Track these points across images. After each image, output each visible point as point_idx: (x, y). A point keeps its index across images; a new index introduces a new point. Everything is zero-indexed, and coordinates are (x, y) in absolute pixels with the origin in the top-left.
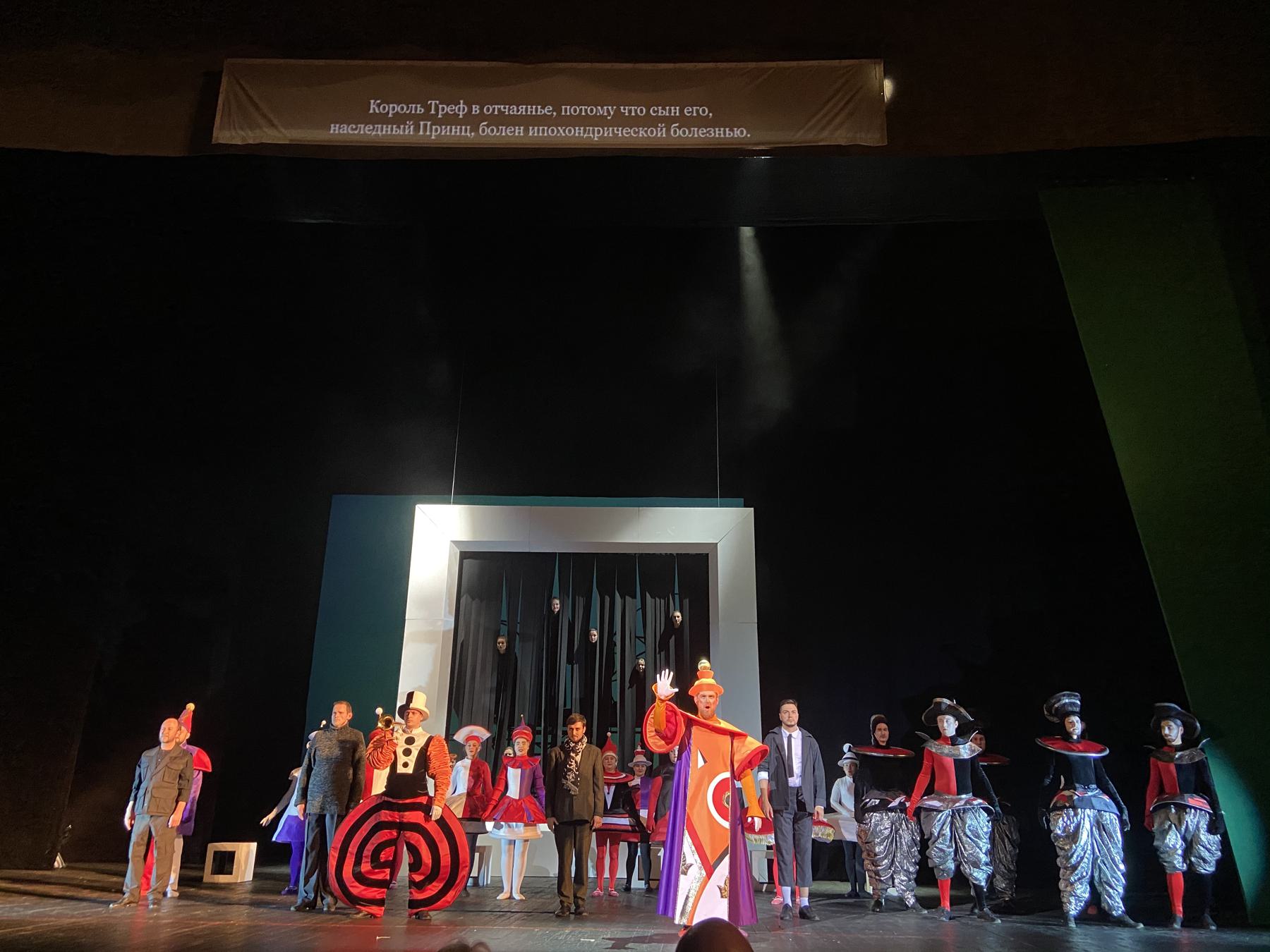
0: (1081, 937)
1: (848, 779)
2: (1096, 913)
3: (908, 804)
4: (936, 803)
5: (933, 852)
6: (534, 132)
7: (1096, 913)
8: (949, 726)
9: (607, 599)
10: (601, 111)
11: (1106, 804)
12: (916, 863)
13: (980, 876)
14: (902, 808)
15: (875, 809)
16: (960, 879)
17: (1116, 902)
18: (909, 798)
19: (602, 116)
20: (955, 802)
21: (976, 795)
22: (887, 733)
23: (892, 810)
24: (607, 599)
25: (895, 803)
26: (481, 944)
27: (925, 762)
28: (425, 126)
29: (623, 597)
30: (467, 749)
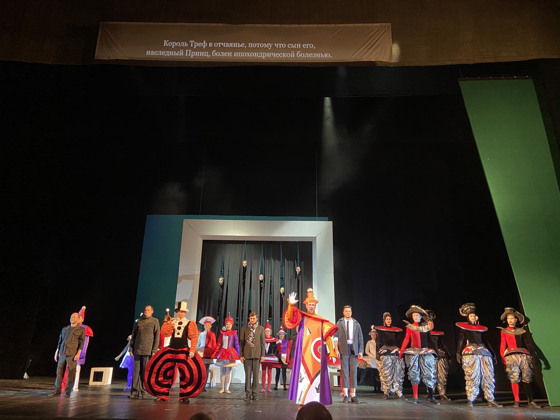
0: (475, 411)
3: (399, 352)
5: (410, 373)
7: (481, 399)
8: (417, 318)
12: (403, 378)
15: (385, 354)
16: (422, 385)
21: (430, 348)
23: (392, 355)
28: (188, 52)
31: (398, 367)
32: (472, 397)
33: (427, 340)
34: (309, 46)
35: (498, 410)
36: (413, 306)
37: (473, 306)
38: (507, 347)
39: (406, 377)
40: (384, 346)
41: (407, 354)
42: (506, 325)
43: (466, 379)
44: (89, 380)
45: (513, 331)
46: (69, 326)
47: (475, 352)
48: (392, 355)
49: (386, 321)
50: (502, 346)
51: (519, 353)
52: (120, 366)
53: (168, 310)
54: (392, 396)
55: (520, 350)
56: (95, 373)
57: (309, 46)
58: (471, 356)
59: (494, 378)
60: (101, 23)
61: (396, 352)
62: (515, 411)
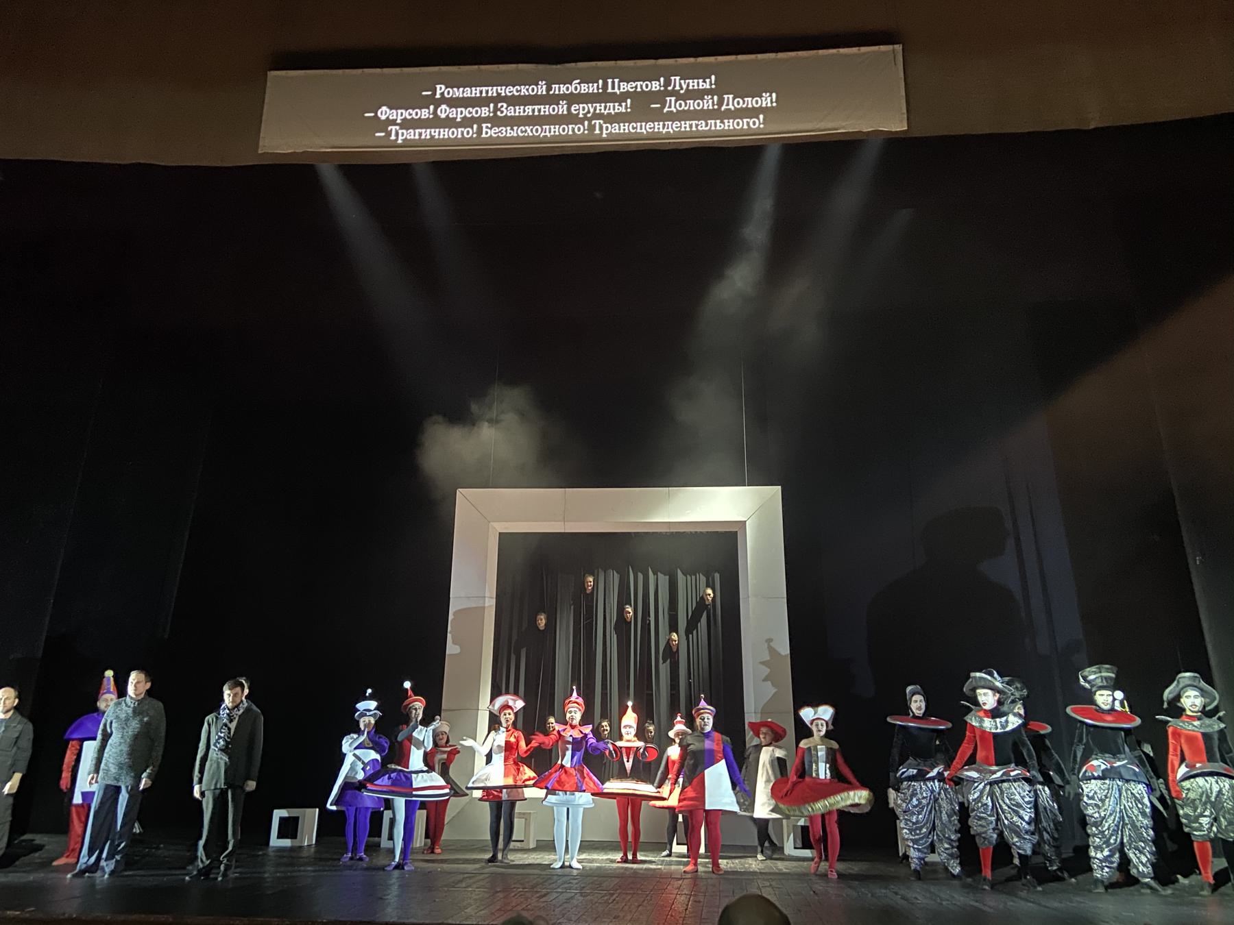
0: (1107, 906)
1: (721, 766)
2: (1125, 877)
3: (946, 774)
4: (974, 774)
5: (972, 822)
7: (1125, 877)
8: (988, 699)
9: (640, 576)
10: (412, 135)
11: (1135, 773)
12: (956, 831)
13: (1023, 846)
14: (940, 777)
15: (911, 778)
16: (1003, 849)
18: (948, 766)
22: (923, 705)
23: (932, 779)
24: (640, 576)
25: (933, 773)
26: (539, 917)
28: (613, 83)
29: (655, 573)
32: (1102, 872)
33: (1008, 750)
34: (748, 123)
37: (1107, 670)
38: (1183, 760)
39: (964, 828)
40: (911, 760)
42: (1176, 710)
45: (1196, 723)
47: (1107, 774)
48: (932, 779)
49: (914, 706)
50: (1173, 758)
51: (1211, 774)
52: (328, 806)
53: (407, 685)
54: (927, 873)
55: (1219, 766)
56: (282, 820)
57: (748, 123)
59: (91, 708)
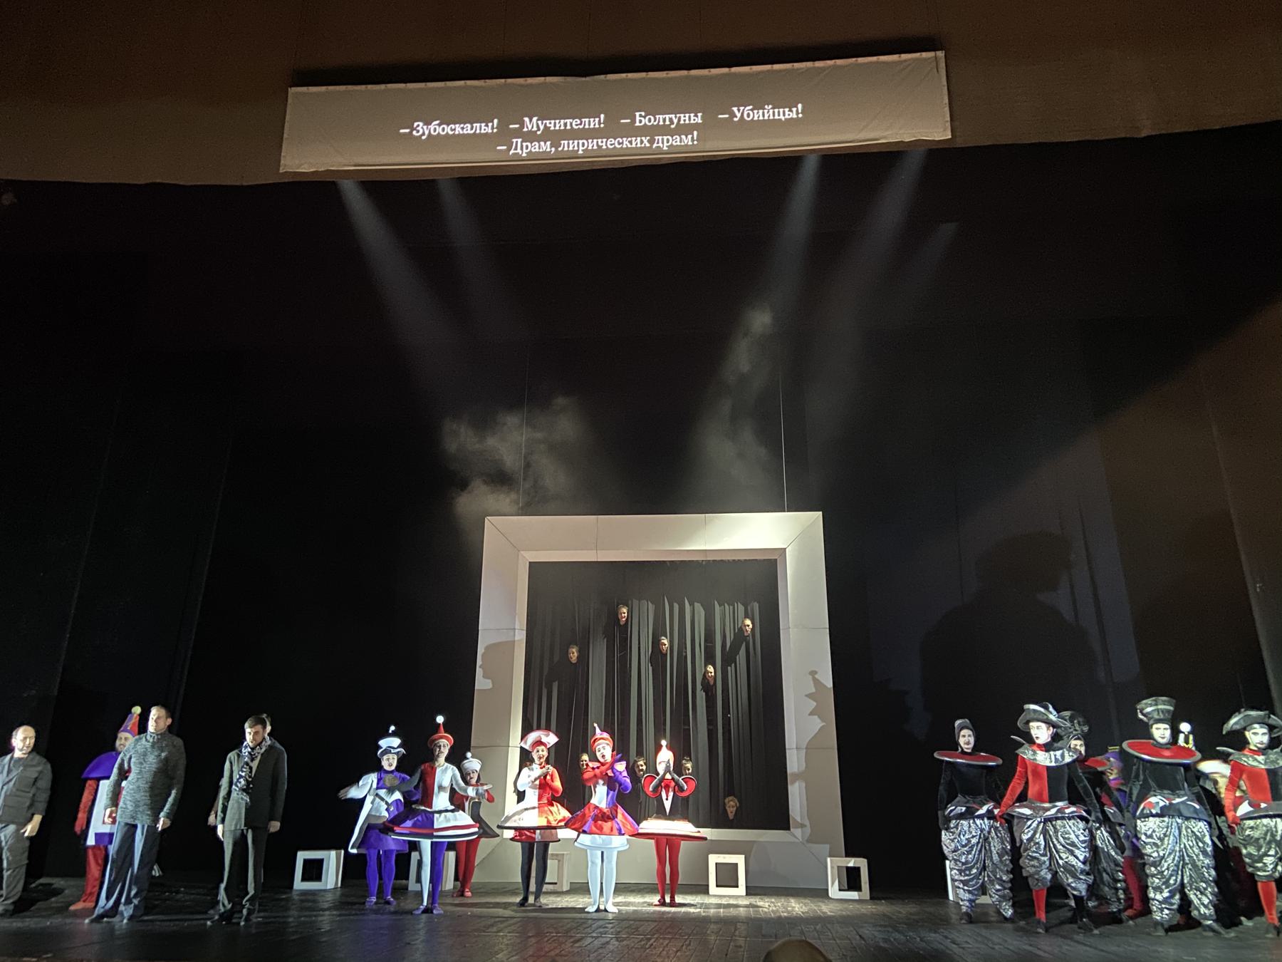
0: (1169, 948)
2: (1186, 918)
3: (996, 811)
4: (1027, 811)
6: (567, 145)
7: (1186, 918)
8: (1041, 733)
9: (676, 606)
11: (1195, 810)
15: (961, 816)
16: (1057, 890)
17: (1203, 903)
19: (530, 132)
20: (1048, 809)
21: (1072, 803)
22: (972, 740)
23: (981, 817)
24: (676, 606)
25: (983, 811)
27: (1019, 769)
29: (691, 604)
30: (535, 756)
31: (995, 846)
35: (1008, 941)
36: (1033, 707)
39: (1016, 869)
41: (1019, 818)
43: (1213, 872)
44: (407, 878)
45: (1261, 758)
46: (9, 757)
48: (981, 817)
49: (962, 741)
56: (307, 862)
58: (1157, 820)
60: (941, 54)
61: (988, 811)
62: (1047, 945)
